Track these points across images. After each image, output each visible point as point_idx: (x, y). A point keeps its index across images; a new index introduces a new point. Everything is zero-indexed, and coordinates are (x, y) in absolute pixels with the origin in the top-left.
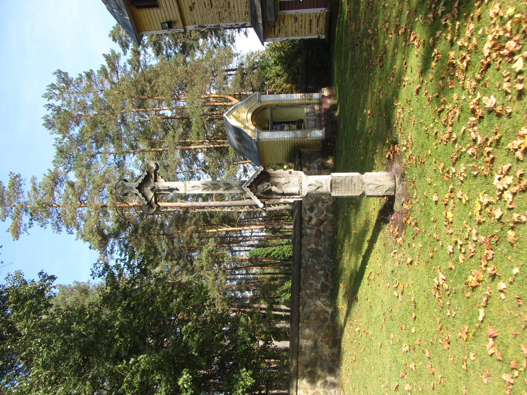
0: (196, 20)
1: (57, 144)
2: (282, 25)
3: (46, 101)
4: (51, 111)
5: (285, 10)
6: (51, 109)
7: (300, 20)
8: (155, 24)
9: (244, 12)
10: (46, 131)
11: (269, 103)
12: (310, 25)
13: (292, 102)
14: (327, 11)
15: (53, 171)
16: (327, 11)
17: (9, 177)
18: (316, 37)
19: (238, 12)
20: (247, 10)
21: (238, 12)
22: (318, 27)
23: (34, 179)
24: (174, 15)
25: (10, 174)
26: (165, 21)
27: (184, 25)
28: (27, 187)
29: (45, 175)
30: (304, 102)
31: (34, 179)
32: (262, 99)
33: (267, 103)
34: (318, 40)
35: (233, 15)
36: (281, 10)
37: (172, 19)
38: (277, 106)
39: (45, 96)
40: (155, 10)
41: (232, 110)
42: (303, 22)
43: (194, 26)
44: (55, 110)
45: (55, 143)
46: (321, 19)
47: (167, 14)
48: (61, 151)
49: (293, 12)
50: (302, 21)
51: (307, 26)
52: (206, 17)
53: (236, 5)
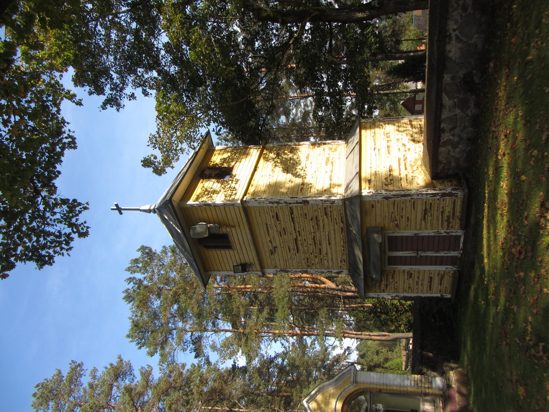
0: (278, 263)
1: (134, 317)
2: (391, 280)
3: (129, 275)
4: (132, 284)
5: (395, 265)
6: (132, 283)
7: (416, 276)
8: (227, 265)
9: (339, 260)
10: (124, 303)
11: (368, 386)
12: (430, 282)
13: (402, 389)
14: (455, 269)
15: (115, 364)
16: (455, 269)
17: (70, 366)
18: (439, 295)
19: (332, 259)
20: (344, 257)
21: (332, 259)
22: (441, 284)
23: (95, 370)
24: (250, 256)
25: (71, 362)
26: (239, 263)
27: (262, 267)
28: (86, 380)
29: (106, 368)
30: (420, 390)
31: (95, 370)
32: (359, 380)
33: (365, 386)
34: (440, 300)
35: (326, 262)
36: (389, 264)
37: (248, 261)
38: (380, 391)
39: (129, 269)
40: (227, 252)
41: (316, 393)
42: (421, 278)
43: (275, 270)
44: (136, 284)
45: (131, 316)
46: (446, 277)
47: (241, 256)
48: (136, 325)
49: (407, 268)
50: (418, 278)
51: (426, 283)
52: (290, 261)
53: (329, 251)
